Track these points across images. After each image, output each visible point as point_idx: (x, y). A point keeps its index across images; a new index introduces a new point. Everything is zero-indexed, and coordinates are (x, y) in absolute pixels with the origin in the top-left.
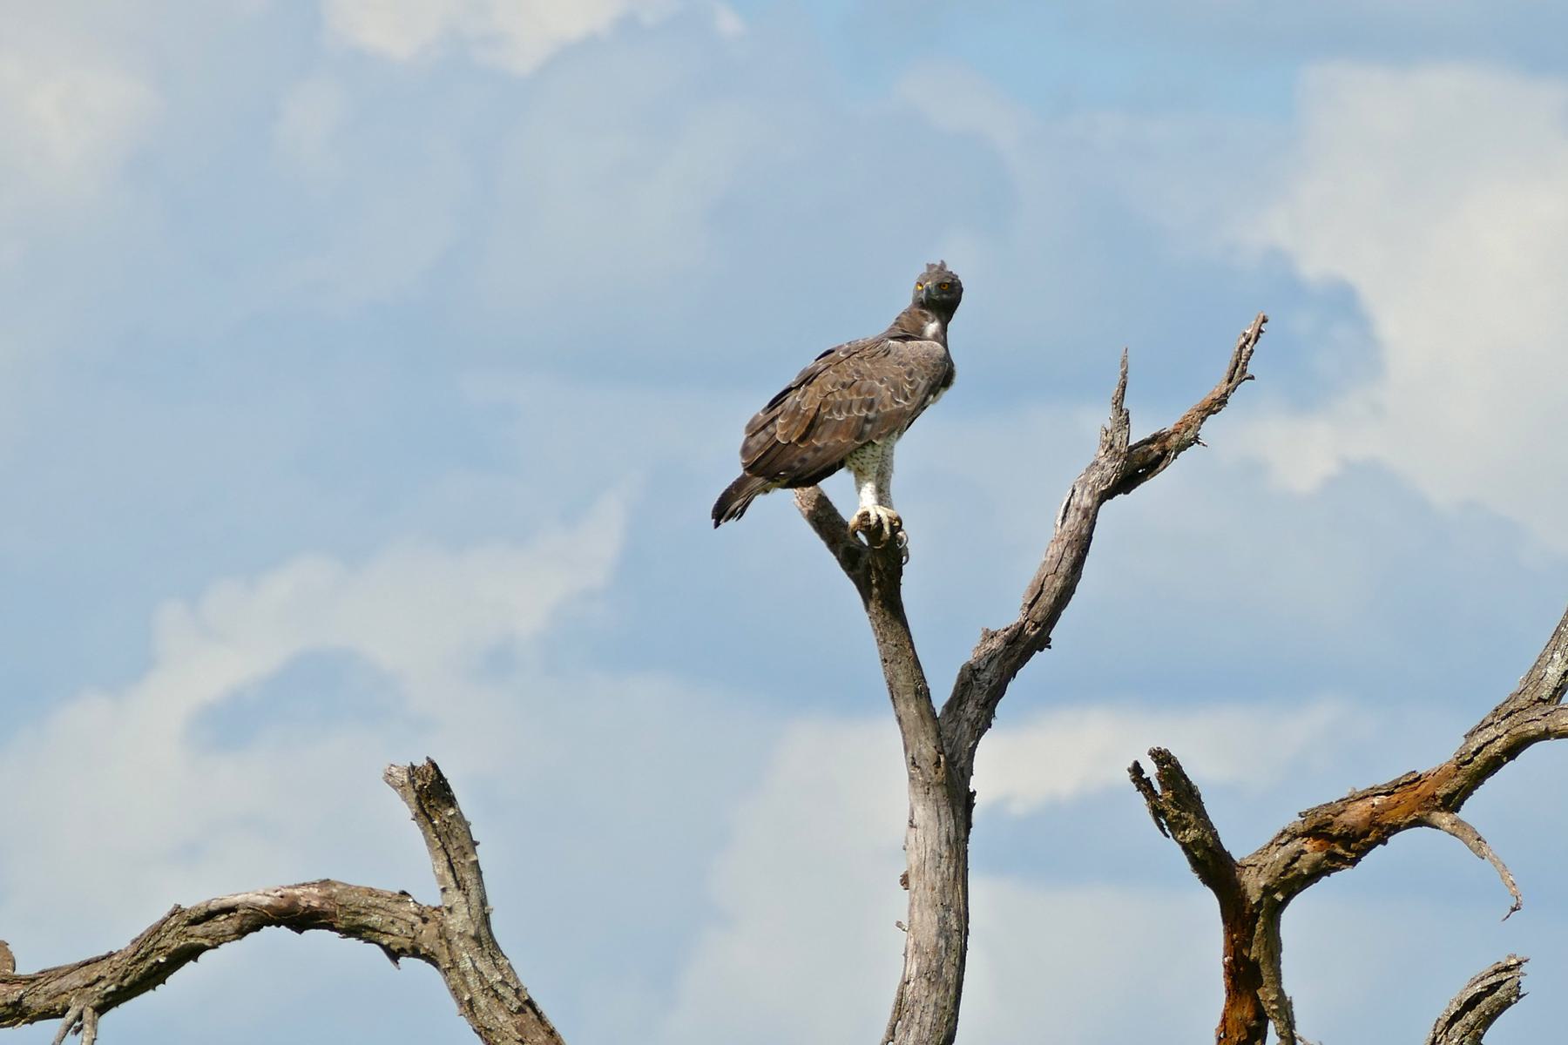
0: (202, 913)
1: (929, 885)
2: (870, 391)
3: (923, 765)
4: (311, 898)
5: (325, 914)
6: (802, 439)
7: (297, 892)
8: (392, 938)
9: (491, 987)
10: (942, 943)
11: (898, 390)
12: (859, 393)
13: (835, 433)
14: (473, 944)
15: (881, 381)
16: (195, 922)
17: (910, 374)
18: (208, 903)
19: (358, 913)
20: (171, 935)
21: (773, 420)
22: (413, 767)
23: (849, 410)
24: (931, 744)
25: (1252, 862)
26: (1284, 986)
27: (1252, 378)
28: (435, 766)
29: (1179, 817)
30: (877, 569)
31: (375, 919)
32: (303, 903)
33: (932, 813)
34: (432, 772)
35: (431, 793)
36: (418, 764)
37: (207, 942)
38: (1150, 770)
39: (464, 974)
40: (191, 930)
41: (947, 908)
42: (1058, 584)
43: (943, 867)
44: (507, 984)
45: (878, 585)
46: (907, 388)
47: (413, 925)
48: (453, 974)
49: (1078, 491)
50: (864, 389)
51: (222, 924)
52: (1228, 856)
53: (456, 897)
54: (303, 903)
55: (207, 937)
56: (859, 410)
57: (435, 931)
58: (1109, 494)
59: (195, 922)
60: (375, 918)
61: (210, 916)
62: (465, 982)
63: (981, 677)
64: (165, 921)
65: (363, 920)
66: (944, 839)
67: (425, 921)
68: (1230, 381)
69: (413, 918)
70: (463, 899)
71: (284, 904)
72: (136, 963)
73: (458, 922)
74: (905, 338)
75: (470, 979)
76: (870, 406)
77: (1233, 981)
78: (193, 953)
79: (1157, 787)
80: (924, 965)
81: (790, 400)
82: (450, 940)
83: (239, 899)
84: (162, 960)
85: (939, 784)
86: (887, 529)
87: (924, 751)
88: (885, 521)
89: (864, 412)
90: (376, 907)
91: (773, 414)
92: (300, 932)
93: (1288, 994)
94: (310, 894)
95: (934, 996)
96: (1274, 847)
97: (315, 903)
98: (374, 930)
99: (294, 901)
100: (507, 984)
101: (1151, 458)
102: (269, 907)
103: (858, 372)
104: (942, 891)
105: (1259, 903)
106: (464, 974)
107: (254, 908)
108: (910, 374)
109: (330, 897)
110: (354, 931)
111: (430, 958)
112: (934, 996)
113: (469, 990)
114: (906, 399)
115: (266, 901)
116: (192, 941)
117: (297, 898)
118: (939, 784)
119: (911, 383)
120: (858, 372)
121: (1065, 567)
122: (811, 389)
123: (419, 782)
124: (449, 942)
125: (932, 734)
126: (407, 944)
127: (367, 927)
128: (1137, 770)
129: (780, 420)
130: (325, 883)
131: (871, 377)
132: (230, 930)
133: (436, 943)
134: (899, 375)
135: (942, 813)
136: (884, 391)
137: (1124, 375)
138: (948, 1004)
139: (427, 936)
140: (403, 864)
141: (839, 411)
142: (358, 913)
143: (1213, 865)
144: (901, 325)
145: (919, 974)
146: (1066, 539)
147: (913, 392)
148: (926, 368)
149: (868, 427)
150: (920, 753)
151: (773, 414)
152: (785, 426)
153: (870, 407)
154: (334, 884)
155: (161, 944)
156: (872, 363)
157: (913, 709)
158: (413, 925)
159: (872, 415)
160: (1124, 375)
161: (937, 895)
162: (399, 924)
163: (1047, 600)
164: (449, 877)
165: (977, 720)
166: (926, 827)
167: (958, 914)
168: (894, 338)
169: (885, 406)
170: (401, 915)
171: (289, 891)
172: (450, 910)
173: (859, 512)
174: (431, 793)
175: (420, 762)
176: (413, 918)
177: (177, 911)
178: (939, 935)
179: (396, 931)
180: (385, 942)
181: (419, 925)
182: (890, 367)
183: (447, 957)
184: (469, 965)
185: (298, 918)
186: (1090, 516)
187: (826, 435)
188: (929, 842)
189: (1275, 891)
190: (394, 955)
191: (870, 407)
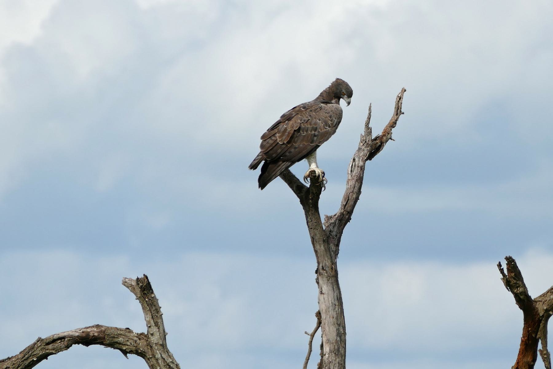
0: (52, 339)
1: (331, 316)
2: (316, 124)
3: (327, 269)
4: (94, 332)
5: (100, 338)
6: (289, 142)
7: (89, 330)
8: (127, 347)
9: (168, 365)
10: (338, 339)
11: (326, 124)
12: (311, 125)
13: (302, 140)
14: (161, 347)
15: (319, 120)
16: (48, 344)
17: (330, 117)
18: (53, 336)
19: (114, 337)
20: (40, 348)
21: (274, 135)
22: (138, 278)
23: (307, 131)
24: (329, 261)
25: (540, 300)
26: (548, 348)
27: (403, 113)
28: (147, 278)
29: (516, 283)
30: (313, 193)
31: (121, 339)
32: (91, 334)
33: (331, 288)
34: (146, 280)
35: (144, 289)
36: (140, 277)
37: (54, 352)
38: (504, 266)
39: (157, 360)
40: (47, 347)
41: (339, 325)
42: (354, 196)
43: (337, 309)
44: (173, 363)
45: (312, 199)
46: (330, 122)
47: (136, 341)
48: (153, 360)
49: (357, 159)
50: (313, 123)
51: (58, 344)
52: (530, 297)
53: (154, 329)
54: (91, 334)
55: (54, 349)
56: (311, 131)
57: (145, 343)
58: (367, 160)
59: (48, 344)
60: (121, 339)
61: (54, 341)
62: (158, 363)
63: (332, 234)
64: (35, 344)
65: (116, 340)
66: (336, 298)
67: (140, 339)
68: (397, 115)
69: (135, 338)
70: (158, 330)
71: (84, 335)
72: (23, 361)
73: (154, 339)
74: (326, 103)
75: (160, 361)
76: (315, 130)
77: (526, 348)
78: (45, 356)
79: (506, 272)
80: (332, 348)
81: (281, 126)
82: (148, 345)
83: (66, 334)
84: (35, 359)
85: (333, 276)
86: (321, 177)
87: (327, 264)
88: (321, 174)
89: (313, 132)
90: (121, 334)
91: (273, 132)
92: (87, 346)
93: (549, 351)
94: (94, 331)
95: (338, 360)
96: (549, 294)
97: (96, 334)
98: (120, 344)
99: (88, 334)
100: (173, 363)
101: (378, 145)
102: (78, 336)
103: (310, 116)
104: (337, 319)
105: (543, 316)
106: (157, 360)
107: (71, 337)
108: (330, 117)
109: (101, 331)
110: (112, 345)
111: (142, 354)
112: (338, 360)
113: (159, 366)
114: (329, 127)
115: (77, 334)
116: (48, 351)
117: (89, 332)
118: (333, 276)
119: (331, 121)
120: (310, 116)
121: (356, 190)
122: (291, 122)
123: (141, 284)
124: (151, 347)
125: (329, 257)
126: (134, 349)
127: (117, 343)
128: (500, 265)
129: (277, 135)
130: (98, 326)
131: (315, 118)
132: (63, 346)
133: (146, 348)
134: (326, 117)
135: (334, 287)
136: (320, 124)
137: (370, 114)
138: (342, 363)
139: (142, 345)
140: (132, 318)
141: (303, 131)
142: (114, 337)
143: (524, 301)
144: (323, 96)
145: (331, 351)
146: (355, 178)
147: (332, 124)
148: (336, 115)
149: (315, 138)
150: (326, 265)
151: (273, 132)
152: (280, 137)
153: (315, 131)
154: (102, 326)
155: (35, 353)
156: (316, 113)
157: (322, 248)
158: (136, 341)
159: (316, 133)
160: (370, 114)
161: (335, 320)
162: (130, 341)
163: (351, 203)
164: (152, 322)
165: (336, 251)
166: (328, 294)
167: (343, 326)
168: (323, 103)
169: (321, 130)
170: (131, 337)
171: (85, 330)
172: (152, 335)
173: (310, 170)
174: (144, 289)
175: (141, 276)
176: (135, 338)
177: (40, 340)
178: (337, 335)
179: (129, 344)
180: (124, 348)
181: (138, 341)
182: (322, 114)
183: (150, 353)
184: (159, 356)
185: (86, 340)
186: (362, 169)
187: (299, 141)
188: (330, 299)
189: (550, 311)
190: (125, 353)
191: (315, 131)
